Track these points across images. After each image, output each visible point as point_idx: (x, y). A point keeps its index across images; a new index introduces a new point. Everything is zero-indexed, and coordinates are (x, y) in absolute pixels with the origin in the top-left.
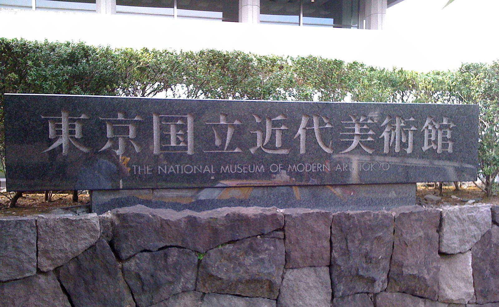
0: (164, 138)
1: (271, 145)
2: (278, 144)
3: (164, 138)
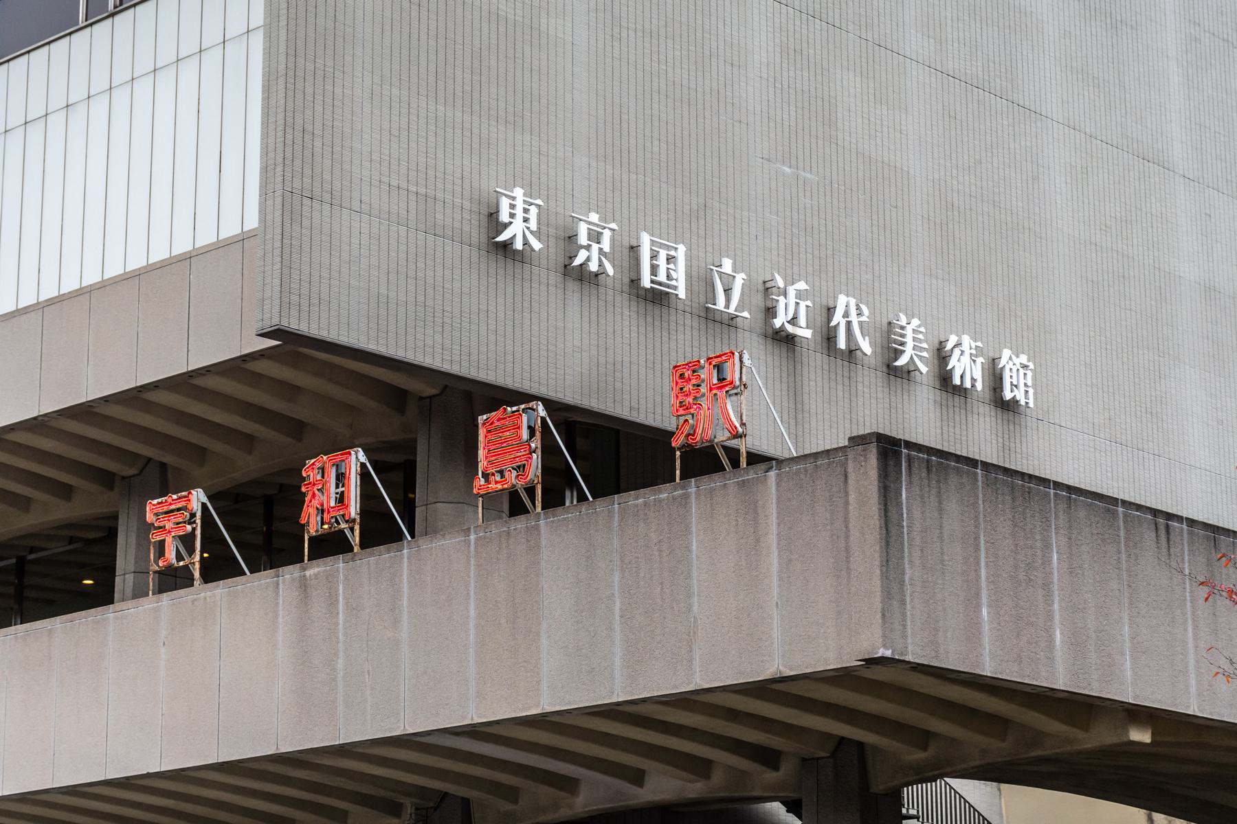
0: (654, 270)
1: (793, 321)
2: (802, 321)
3: (654, 270)
